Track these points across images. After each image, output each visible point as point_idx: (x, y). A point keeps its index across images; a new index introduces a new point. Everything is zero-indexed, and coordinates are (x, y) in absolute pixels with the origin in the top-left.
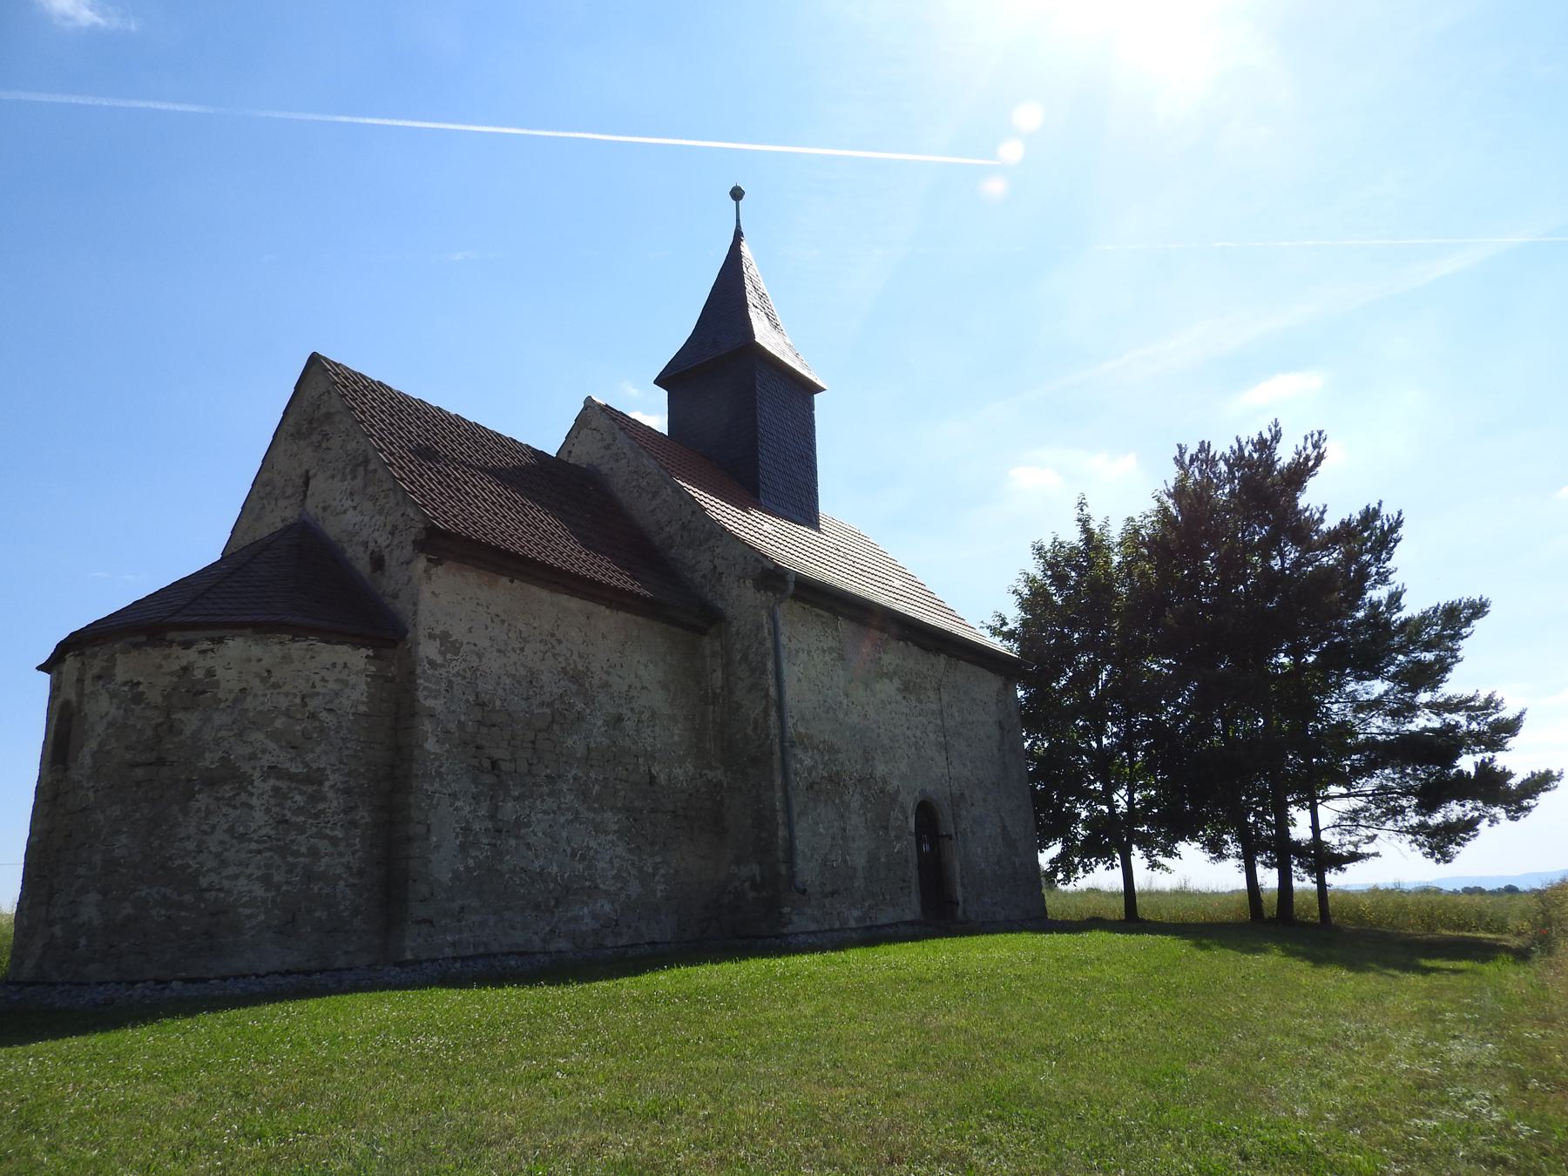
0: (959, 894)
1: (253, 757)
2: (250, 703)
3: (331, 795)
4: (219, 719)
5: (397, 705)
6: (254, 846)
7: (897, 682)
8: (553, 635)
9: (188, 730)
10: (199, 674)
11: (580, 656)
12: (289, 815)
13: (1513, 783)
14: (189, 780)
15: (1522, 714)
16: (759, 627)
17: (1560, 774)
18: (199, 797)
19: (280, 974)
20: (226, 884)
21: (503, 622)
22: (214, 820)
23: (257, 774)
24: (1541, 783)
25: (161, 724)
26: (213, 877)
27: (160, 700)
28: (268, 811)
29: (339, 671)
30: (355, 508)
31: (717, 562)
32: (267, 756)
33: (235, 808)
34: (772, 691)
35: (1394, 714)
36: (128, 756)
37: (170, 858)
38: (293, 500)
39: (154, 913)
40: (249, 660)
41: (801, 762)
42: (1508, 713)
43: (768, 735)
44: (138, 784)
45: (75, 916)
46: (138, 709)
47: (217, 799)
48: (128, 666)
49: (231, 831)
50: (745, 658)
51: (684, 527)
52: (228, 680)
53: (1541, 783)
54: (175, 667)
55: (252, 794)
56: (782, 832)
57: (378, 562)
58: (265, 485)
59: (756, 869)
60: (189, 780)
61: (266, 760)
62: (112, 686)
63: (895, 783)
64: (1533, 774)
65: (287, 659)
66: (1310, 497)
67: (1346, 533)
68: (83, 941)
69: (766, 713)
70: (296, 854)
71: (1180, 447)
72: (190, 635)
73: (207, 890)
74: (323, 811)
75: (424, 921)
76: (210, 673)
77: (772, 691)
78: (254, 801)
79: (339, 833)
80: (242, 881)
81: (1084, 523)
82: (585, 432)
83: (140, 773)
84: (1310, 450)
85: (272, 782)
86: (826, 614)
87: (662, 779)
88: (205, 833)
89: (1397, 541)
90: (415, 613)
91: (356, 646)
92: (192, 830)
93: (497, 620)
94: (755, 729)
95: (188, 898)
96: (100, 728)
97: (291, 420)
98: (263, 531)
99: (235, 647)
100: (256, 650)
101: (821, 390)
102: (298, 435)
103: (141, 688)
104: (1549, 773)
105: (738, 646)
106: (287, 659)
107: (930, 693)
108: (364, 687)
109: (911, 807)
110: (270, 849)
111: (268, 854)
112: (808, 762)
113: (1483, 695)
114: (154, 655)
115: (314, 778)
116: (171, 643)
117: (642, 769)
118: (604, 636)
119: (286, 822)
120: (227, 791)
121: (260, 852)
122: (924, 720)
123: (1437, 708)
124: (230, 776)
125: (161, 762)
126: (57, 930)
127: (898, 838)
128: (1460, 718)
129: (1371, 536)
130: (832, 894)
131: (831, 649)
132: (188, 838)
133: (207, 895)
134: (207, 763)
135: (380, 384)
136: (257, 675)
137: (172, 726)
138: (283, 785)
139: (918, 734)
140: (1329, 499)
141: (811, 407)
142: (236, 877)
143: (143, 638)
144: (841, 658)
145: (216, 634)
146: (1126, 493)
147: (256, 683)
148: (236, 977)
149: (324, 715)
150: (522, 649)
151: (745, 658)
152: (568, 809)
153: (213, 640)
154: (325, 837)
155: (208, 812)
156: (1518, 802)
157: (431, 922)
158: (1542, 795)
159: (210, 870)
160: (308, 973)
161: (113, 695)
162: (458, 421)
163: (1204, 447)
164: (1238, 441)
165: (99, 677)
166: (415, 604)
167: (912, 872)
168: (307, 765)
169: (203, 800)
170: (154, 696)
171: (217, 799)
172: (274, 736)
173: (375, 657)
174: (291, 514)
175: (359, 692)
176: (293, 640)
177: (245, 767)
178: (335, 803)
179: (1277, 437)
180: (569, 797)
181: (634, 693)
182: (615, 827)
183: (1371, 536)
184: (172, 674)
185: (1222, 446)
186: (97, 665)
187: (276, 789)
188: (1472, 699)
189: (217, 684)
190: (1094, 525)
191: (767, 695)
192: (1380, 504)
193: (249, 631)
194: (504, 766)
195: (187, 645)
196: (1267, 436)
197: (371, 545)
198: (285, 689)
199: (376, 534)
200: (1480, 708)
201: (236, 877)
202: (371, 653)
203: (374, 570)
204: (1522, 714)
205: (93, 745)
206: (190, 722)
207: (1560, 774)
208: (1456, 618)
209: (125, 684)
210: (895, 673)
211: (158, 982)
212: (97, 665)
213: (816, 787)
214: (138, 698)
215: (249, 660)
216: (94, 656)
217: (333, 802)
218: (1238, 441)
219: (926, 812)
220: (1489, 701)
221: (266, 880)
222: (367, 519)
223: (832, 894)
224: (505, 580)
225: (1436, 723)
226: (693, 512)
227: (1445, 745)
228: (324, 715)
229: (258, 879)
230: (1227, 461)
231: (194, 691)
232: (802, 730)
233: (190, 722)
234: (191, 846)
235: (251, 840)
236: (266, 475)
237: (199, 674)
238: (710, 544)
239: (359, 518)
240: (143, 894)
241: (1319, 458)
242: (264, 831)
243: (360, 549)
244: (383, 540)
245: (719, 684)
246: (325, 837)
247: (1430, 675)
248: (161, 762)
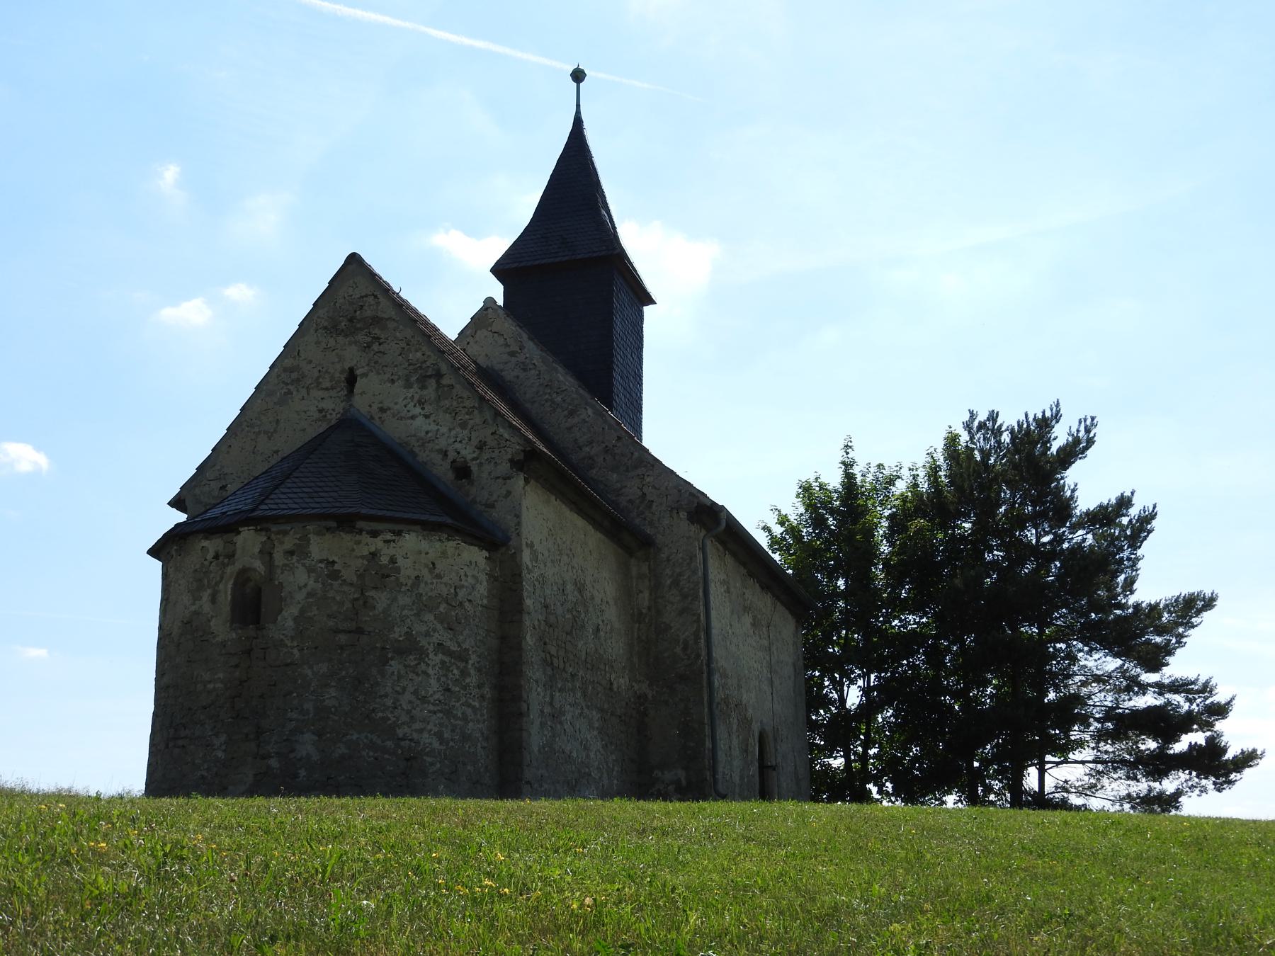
1: (427, 634)
2: (422, 589)
4: (404, 600)
6: (431, 707)
9: (380, 607)
10: (384, 560)
13: (1229, 755)
14: (383, 648)
15: (1233, 699)
16: (692, 558)
17: (1263, 753)
18: (392, 663)
20: (415, 736)
22: (404, 683)
23: (431, 648)
24: (1247, 759)
25: (356, 599)
26: (406, 729)
27: (355, 579)
28: (438, 679)
29: (466, 563)
30: (427, 417)
31: (645, 490)
32: (436, 635)
33: (417, 675)
34: (702, 618)
35: (1118, 690)
36: (331, 623)
37: (373, 710)
38: (333, 393)
39: (364, 753)
40: (420, 552)
42: (1220, 697)
43: (698, 656)
44: (342, 648)
45: (293, 751)
46: (336, 584)
47: (405, 666)
49: (415, 693)
50: (676, 583)
51: (606, 450)
52: (407, 569)
53: (1247, 759)
54: (366, 553)
55: (428, 665)
56: (708, 744)
58: (290, 370)
59: (682, 774)
60: (383, 648)
61: (436, 638)
62: (307, 562)
64: (1243, 752)
65: (444, 554)
66: (1073, 476)
67: (1104, 517)
68: (302, 773)
69: (697, 637)
70: (455, 717)
71: (971, 413)
73: (402, 739)
74: (468, 685)
76: (393, 560)
77: (702, 618)
78: (430, 671)
79: (476, 704)
80: (425, 735)
81: (848, 465)
82: (481, 334)
83: (343, 638)
84: (1082, 434)
88: (398, 693)
89: (1150, 532)
90: (519, 524)
91: (482, 548)
92: (389, 690)
94: (685, 649)
95: (389, 743)
96: (300, 596)
97: (321, 312)
99: (411, 541)
100: (424, 545)
101: (654, 302)
102: (333, 328)
103: (336, 567)
104: (1255, 751)
105: (668, 571)
110: (440, 711)
111: (440, 715)
113: (1202, 680)
114: (347, 539)
115: (462, 657)
116: (360, 532)
120: (411, 659)
121: (435, 713)
123: (1161, 688)
124: (410, 648)
126: (274, 763)
128: (1178, 699)
129: (1122, 528)
132: (386, 696)
133: (402, 743)
134: (396, 636)
137: (365, 602)
138: (447, 659)
140: (1088, 485)
142: (421, 731)
143: (333, 524)
145: (397, 527)
146: (903, 447)
147: (425, 572)
149: (467, 604)
151: (676, 583)
153: (393, 532)
155: (400, 677)
156: (1227, 775)
158: (1247, 771)
159: (403, 723)
161: (310, 570)
163: (993, 416)
164: (1026, 415)
165: (291, 553)
166: (518, 516)
168: (459, 646)
169: (395, 666)
170: (349, 575)
172: (441, 619)
174: (334, 406)
177: (423, 643)
179: (1057, 416)
183: (1122, 528)
184: (363, 557)
185: (1009, 419)
186: (289, 543)
187: (443, 662)
188: (1193, 683)
189: (398, 570)
190: (856, 470)
191: (698, 621)
192: (1133, 493)
193: (418, 528)
195: (374, 534)
196: (1048, 414)
197: (452, 455)
198: (444, 580)
199: (457, 446)
200: (1198, 692)
201: (421, 731)
204: (1233, 699)
205: (295, 610)
206: (381, 600)
207: (1263, 753)
208: (1191, 607)
209: (321, 561)
212: (289, 543)
214: (335, 575)
215: (420, 552)
216: (285, 533)
217: (473, 680)
218: (1026, 415)
220: (1206, 685)
221: (439, 735)
222: (444, 430)
225: (1159, 701)
226: (619, 438)
227: (1165, 724)
228: (467, 604)
229: (435, 734)
230: (1012, 432)
231: (381, 574)
233: (381, 600)
234: (389, 702)
235: (429, 702)
236: (288, 362)
237: (384, 560)
238: (640, 471)
239: (434, 427)
240: (354, 738)
241: (1090, 442)
242: (436, 697)
243: (438, 458)
244: (468, 453)
245: (646, 603)
247: (1155, 660)
248: (360, 631)
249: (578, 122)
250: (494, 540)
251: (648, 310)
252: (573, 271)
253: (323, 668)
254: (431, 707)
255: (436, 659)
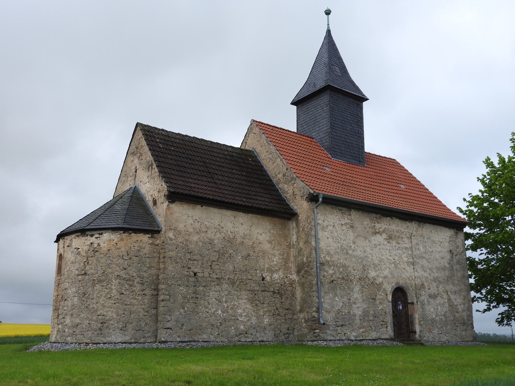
0: (417, 328)
1: (112, 273)
3: (137, 285)
5: (160, 254)
7: (384, 236)
8: (219, 225)
11: (231, 232)
12: (124, 292)
19: (122, 343)
20: (105, 314)
21: (198, 222)
36: (77, 272)
41: (327, 272)
48: (80, 243)
50: (303, 230)
51: (284, 175)
57: (155, 202)
61: (117, 273)
63: (380, 280)
68: (67, 330)
72: (93, 233)
75: (168, 328)
76: (99, 245)
78: (113, 287)
80: (110, 313)
83: (80, 277)
85: (118, 280)
86: (344, 209)
87: (268, 278)
93: (196, 221)
98: (120, 192)
103: (79, 250)
106: (122, 240)
107: (406, 240)
108: (148, 248)
109: (389, 288)
112: (331, 272)
117: (258, 275)
118: (242, 224)
119: (123, 294)
120: (105, 283)
122: (400, 252)
125: (85, 274)
127: (381, 303)
130: (342, 326)
131: (346, 224)
135: (163, 130)
136: (113, 245)
138: (122, 281)
139: (396, 258)
141: (361, 108)
142: (108, 311)
143: (80, 234)
144: (352, 227)
145: (101, 232)
148: (109, 343)
150: (206, 232)
151: (303, 230)
152: (226, 290)
154: (135, 299)
157: (171, 329)
160: (131, 343)
161: (72, 252)
162: (194, 138)
167: (389, 319)
171: (102, 286)
173: (152, 237)
175: (147, 249)
176: (124, 233)
178: (139, 288)
180: (226, 286)
181: (255, 245)
182: (246, 297)
184: (88, 245)
187: (120, 283)
193: (110, 231)
194: (200, 275)
195: (92, 236)
197: (153, 195)
201: (108, 311)
202: (150, 236)
203: (154, 205)
210: (384, 231)
211: (86, 343)
212: (68, 242)
213: (334, 282)
214: (79, 253)
216: (67, 239)
219: (400, 293)
223: (342, 326)
224: (199, 207)
232: (328, 259)
243: (150, 197)
245: (295, 240)
246: (135, 299)
248: (85, 274)
249: (329, 32)
250: (153, 231)
251: (365, 104)
252: (333, 97)
253: (74, 290)
254: (113, 302)
255: (115, 282)
